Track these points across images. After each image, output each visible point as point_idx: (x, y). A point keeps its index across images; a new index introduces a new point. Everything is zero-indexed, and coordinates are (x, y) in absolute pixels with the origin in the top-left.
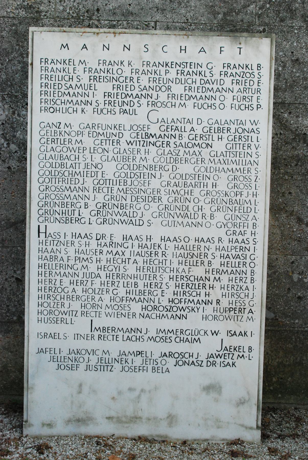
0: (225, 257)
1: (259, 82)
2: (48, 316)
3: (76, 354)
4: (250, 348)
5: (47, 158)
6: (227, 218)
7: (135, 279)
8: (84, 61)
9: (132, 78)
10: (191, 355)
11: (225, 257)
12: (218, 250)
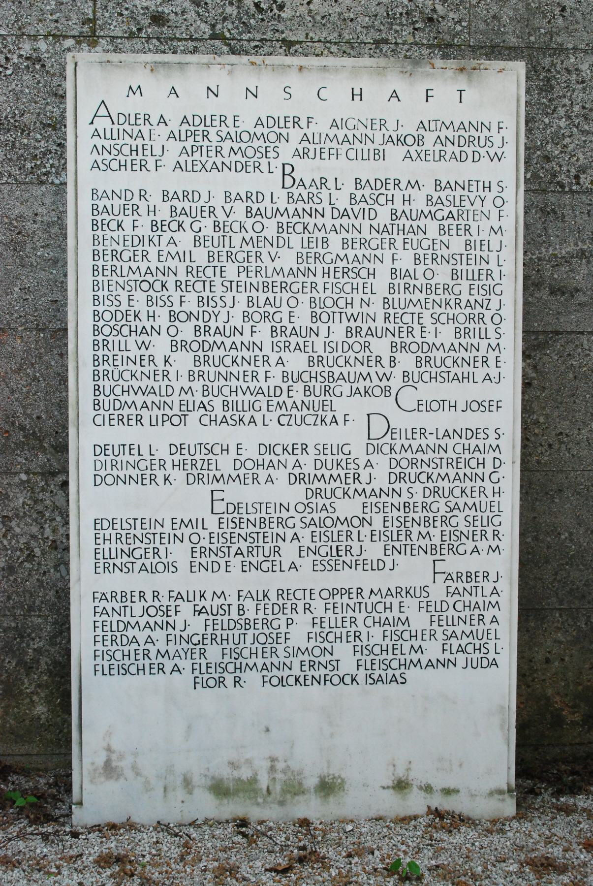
0: (139, 333)
1: (131, 298)
9: (357, 634)
10: (225, 447)
11: (139, 332)
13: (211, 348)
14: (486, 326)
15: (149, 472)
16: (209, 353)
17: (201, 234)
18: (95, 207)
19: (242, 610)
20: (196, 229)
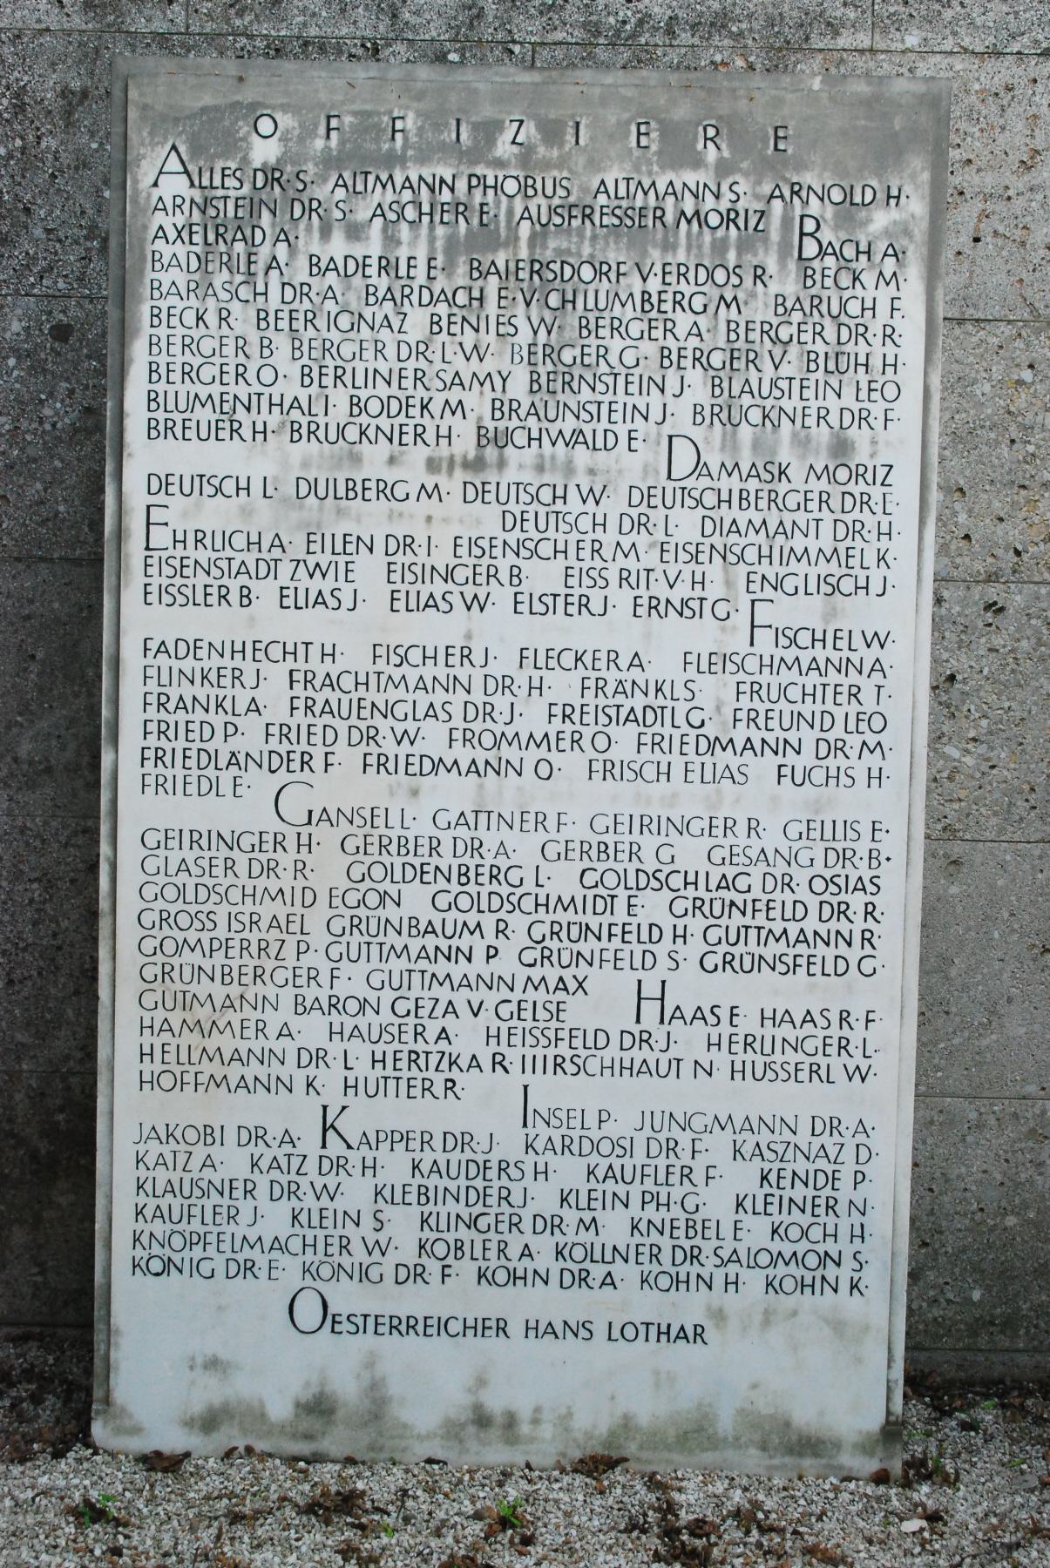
2: (851, 487)
3: (164, 1141)
4: (245, 592)
5: (172, 870)
6: (149, 976)
7: (238, 656)
8: (517, 734)
12: (336, 1038)
13: (178, 951)
14: (896, 350)
15: (411, 1020)
16: (176, 961)
17: (698, 1217)
18: (300, 1000)
19: (247, 596)
20: (690, 1207)
